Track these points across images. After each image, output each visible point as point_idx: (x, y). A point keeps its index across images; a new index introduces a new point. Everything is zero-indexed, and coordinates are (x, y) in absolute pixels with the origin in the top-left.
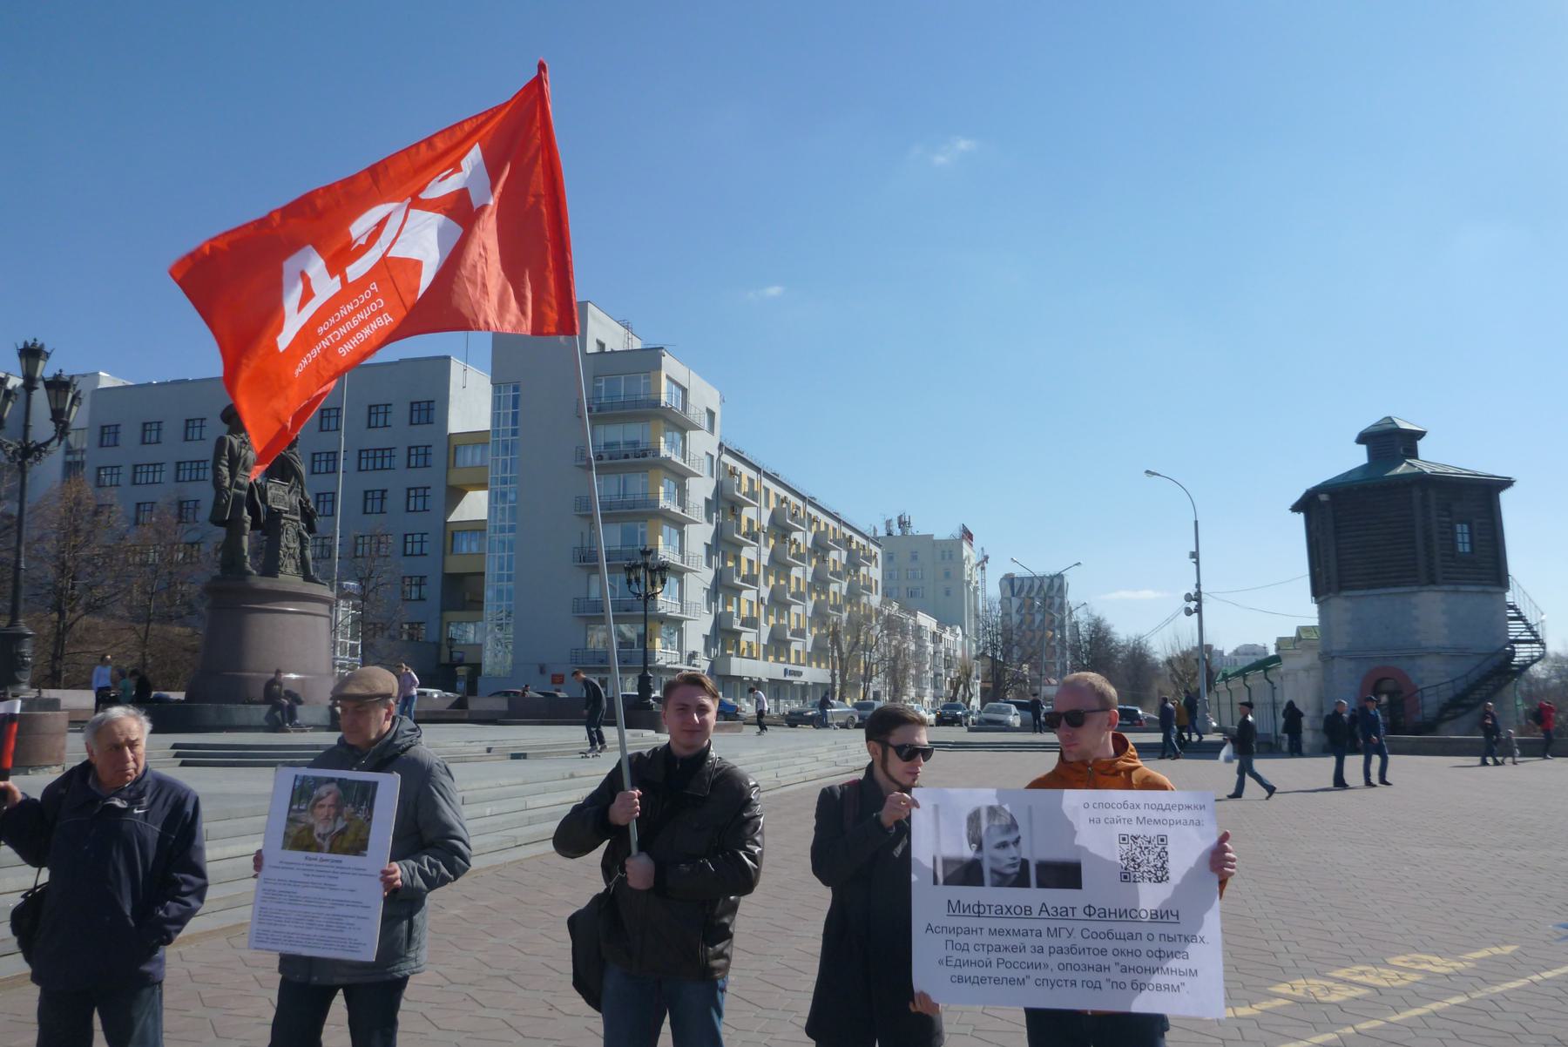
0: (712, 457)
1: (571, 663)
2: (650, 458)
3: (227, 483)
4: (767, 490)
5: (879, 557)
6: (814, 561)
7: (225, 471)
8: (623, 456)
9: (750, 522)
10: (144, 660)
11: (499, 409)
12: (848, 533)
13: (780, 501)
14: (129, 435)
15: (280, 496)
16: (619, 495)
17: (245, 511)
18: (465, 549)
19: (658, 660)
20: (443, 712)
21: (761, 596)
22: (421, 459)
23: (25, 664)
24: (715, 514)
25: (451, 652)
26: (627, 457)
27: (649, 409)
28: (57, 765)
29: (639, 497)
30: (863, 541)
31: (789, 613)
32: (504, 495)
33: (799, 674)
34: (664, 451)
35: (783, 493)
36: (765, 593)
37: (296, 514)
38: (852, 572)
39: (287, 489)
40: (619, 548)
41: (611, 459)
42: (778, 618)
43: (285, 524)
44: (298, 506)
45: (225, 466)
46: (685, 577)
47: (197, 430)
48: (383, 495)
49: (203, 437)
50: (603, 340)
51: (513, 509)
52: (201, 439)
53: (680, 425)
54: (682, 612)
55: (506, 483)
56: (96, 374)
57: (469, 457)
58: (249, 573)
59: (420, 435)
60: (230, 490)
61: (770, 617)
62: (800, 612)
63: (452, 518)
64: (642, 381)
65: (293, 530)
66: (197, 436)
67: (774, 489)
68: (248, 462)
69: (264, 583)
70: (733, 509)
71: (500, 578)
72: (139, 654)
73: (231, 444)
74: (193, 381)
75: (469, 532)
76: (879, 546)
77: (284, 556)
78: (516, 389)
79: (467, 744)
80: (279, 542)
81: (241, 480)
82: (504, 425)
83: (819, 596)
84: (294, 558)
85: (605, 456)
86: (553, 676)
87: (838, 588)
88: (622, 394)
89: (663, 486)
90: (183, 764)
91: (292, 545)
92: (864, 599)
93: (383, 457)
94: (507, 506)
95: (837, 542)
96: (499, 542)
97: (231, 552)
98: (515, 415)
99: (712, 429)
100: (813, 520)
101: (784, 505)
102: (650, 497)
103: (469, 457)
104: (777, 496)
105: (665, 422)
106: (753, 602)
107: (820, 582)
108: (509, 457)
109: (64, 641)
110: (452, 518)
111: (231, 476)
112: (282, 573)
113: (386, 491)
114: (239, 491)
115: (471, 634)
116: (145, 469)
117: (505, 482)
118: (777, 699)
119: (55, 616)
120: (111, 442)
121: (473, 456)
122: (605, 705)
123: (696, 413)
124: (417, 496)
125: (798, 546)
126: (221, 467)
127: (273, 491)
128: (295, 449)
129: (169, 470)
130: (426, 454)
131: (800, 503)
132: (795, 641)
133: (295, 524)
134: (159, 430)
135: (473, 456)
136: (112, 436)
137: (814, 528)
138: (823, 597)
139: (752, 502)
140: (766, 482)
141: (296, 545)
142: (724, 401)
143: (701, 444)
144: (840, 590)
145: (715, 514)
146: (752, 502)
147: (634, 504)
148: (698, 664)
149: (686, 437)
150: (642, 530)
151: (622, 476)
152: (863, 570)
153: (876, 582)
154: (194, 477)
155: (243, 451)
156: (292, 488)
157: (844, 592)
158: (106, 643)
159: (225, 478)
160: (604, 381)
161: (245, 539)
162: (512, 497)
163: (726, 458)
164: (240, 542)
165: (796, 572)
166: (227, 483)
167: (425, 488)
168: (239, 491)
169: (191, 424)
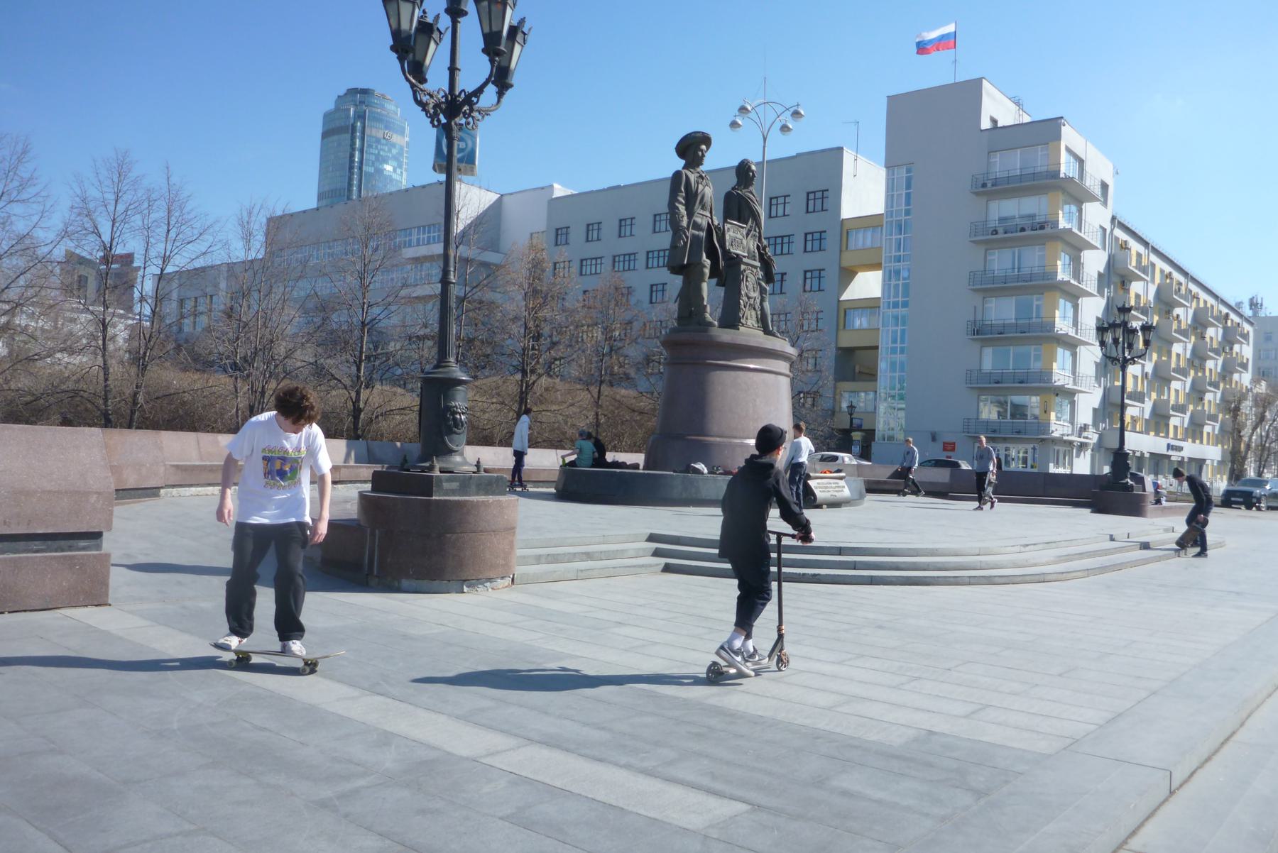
0: (1104, 230)
1: (964, 432)
2: (1048, 230)
3: (685, 222)
4: (1153, 265)
5: (1251, 335)
6: (1193, 338)
7: (682, 209)
8: (1019, 229)
9: (1138, 296)
10: (597, 419)
11: (893, 190)
12: (1225, 310)
13: (1164, 277)
14: (577, 235)
15: (738, 239)
16: (1014, 268)
17: (704, 255)
18: (857, 323)
19: (1053, 432)
20: (885, 482)
21: (1145, 371)
22: (816, 244)
23: (457, 424)
24: (1106, 290)
25: (851, 419)
26: (1023, 230)
27: (1048, 181)
28: (503, 578)
29: (1036, 270)
30: (1236, 319)
31: (1169, 389)
32: (898, 273)
33: (1180, 449)
34: (1063, 224)
35: (1168, 269)
36: (1149, 367)
37: (755, 260)
38: (1227, 349)
39: (744, 232)
40: (1013, 321)
41: (1006, 233)
42: (1160, 393)
43: (745, 271)
44: (756, 251)
45: (681, 203)
46: (1078, 350)
47: (628, 228)
48: (782, 278)
49: (633, 234)
50: (996, 117)
51: (906, 286)
52: (631, 235)
53: (1076, 194)
54: (1075, 383)
55: (899, 261)
56: (551, 186)
57: (861, 240)
58: (711, 324)
59: (815, 222)
60: (688, 231)
61: (1152, 393)
62: (1180, 387)
63: (843, 298)
64: (1040, 153)
65: (753, 278)
66: (628, 233)
67: (1160, 265)
68: (705, 199)
69: (726, 336)
70: (1123, 283)
71: (894, 351)
72: (593, 413)
73: (687, 178)
74: (625, 186)
75: (860, 310)
76: (1251, 324)
77: (745, 307)
78: (908, 171)
79: (1023, 549)
80: (740, 290)
81: (699, 220)
82: (897, 206)
83: (1196, 373)
84: (754, 309)
85: (1001, 230)
86: (944, 443)
87: (1213, 365)
88: (1018, 167)
89: (1060, 260)
90: (668, 569)
91: (752, 294)
92: (1236, 377)
93: (782, 244)
94: (900, 282)
95: (1217, 319)
96: (892, 317)
97: (689, 299)
98: (908, 195)
99: (1105, 203)
100: (1196, 297)
101: (1168, 281)
102: (1048, 269)
103: (861, 240)
104: (1162, 271)
105: (1063, 193)
106: (1137, 377)
107: (1198, 359)
108: (902, 237)
109: (527, 399)
110: (843, 298)
111: (687, 214)
112: (743, 325)
113: (785, 274)
114: (696, 233)
115: (863, 400)
116: (589, 262)
117: (898, 259)
118: (1156, 474)
119: (519, 376)
120: (563, 242)
121: (864, 238)
122: (1205, 498)
123: (1092, 184)
124: (814, 276)
125: (1180, 322)
126: (677, 204)
127: (731, 233)
128: (751, 188)
129: (607, 262)
130: (821, 239)
131: (1182, 279)
132: (1174, 416)
133: (755, 271)
134: (599, 229)
135: (864, 238)
136: (564, 236)
137: (1194, 304)
138: (1200, 374)
139: (1143, 275)
140: (1154, 258)
141: (756, 294)
142: (1117, 173)
143: (1096, 216)
144: (1216, 368)
145: (1106, 290)
146: (1143, 275)
147: (1031, 277)
148: (1090, 436)
149: (1082, 209)
150: (1038, 303)
151: (1017, 250)
152: (1236, 348)
153: (1248, 359)
154: (626, 268)
155: (700, 187)
156: (749, 231)
157: (1219, 370)
158: (564, 402)
159: (683, 216)
160: (998, 155)
161: (705, 286)
162: (904, 274)
163: (1119, 233)
164: (699, 289)
165: (1177, 348)
166: (685, 222)
167: (820, 270)
168: (696, 233)
169: (623, 223)
